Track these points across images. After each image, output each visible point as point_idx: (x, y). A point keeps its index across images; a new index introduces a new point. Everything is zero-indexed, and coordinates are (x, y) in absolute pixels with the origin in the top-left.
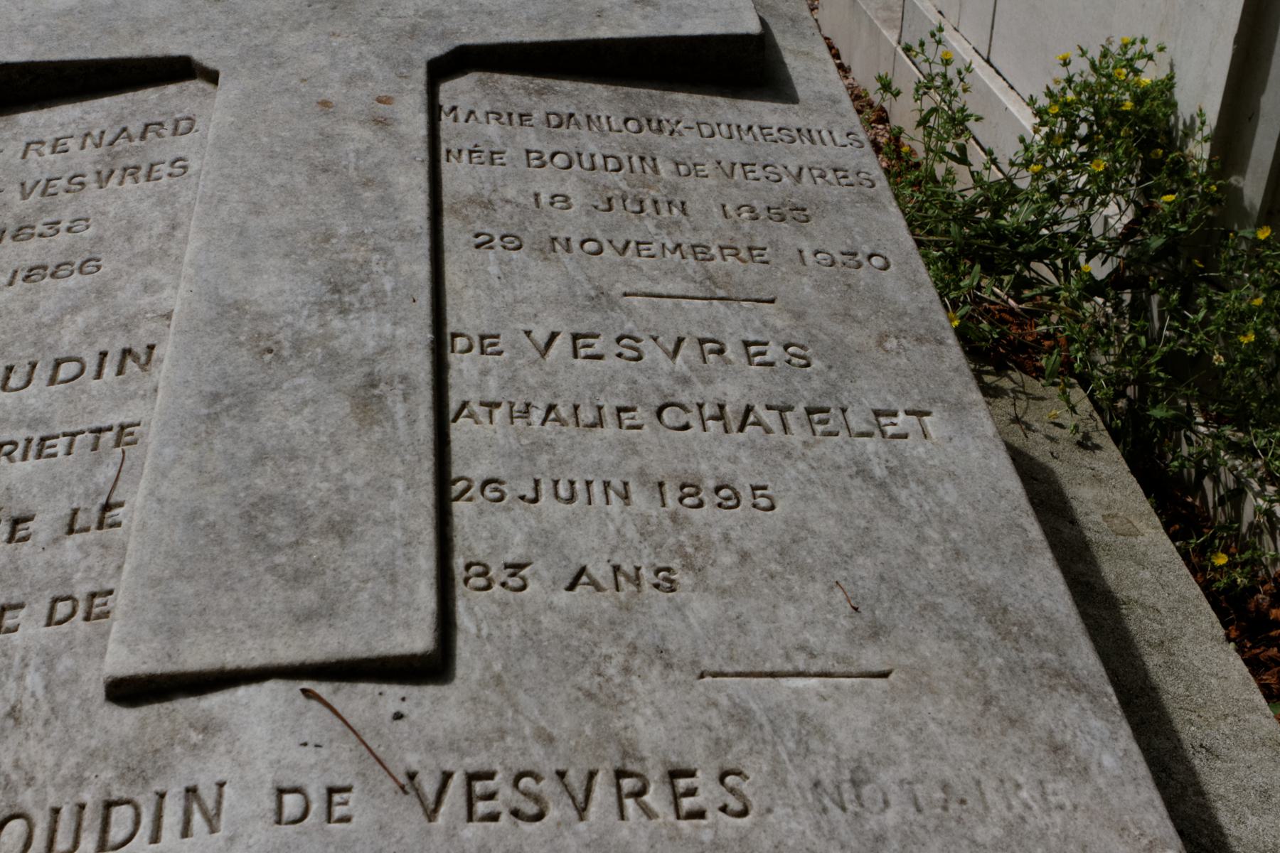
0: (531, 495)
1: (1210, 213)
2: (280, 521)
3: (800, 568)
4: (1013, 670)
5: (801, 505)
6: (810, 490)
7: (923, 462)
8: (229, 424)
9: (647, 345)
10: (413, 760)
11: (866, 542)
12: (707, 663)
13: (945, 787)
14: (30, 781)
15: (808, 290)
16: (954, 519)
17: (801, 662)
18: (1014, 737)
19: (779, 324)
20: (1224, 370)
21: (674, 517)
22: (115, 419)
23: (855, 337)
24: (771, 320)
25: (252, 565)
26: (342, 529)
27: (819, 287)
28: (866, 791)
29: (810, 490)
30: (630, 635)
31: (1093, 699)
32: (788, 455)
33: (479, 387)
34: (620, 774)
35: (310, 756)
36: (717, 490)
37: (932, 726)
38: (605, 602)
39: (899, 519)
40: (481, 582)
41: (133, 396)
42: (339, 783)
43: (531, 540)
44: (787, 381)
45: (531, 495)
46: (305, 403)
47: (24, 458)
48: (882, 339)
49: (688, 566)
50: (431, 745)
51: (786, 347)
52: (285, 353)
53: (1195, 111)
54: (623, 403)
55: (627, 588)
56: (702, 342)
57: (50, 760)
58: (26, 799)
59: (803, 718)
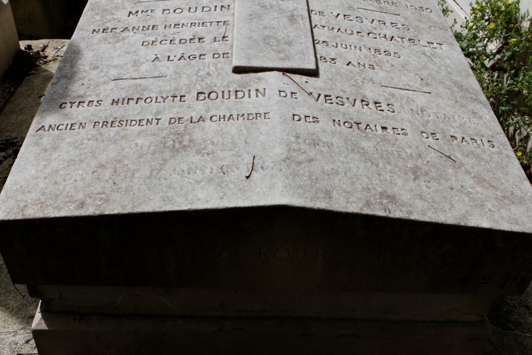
0: (335, 46)
1: (527, 45)
2: (272, 41)
3: (407, 70)
4: (463, 97)
5: (407, 58)
6: (410, 55)
7: (441, 54)
8: (256, 21)
9: (364, 20)
10: (311, 90)
11: (425, 67)
12: (383, 84)
13: (445, 115)
14: (216, 86)
15: (409, 14)
16: (449, 66)
17: (408, 88)
18: (463, 109)
19: (401, 20)
20: (527, 97)
21: (373, 55)
22: (223, 20)
23: (422, 25)
24: (399, 19)
25: (267, 48)
26: (289, 44)
27: (412, 13)
28: (424, 113)
29: (410, 55)
30: (363, 76)
31: (484, 105)
32: (404, 48)
33: (320, 22)
34: (362, 101)
35: (286, 86)
36: (385, 52)
37: (442, 104)
38: (357, 69)
39: (434, 64)
40: (325, 61)
41: (226, 15)
42: (294, 92)
43: (336, 54)
44: (403, 32)
45: (335, 46)
46: (275, 18)
47: (199, 26)
48: (430, 27)
49: (378, 65)
50: (315, 88)
51: (403, 25)
52: (268, 7)
53: (525, 11)
54: (359, 31)
55: (362, 68)
56: (380, 21)
57: (220, 82)
58: (215, 89)
59: (408, 98)
